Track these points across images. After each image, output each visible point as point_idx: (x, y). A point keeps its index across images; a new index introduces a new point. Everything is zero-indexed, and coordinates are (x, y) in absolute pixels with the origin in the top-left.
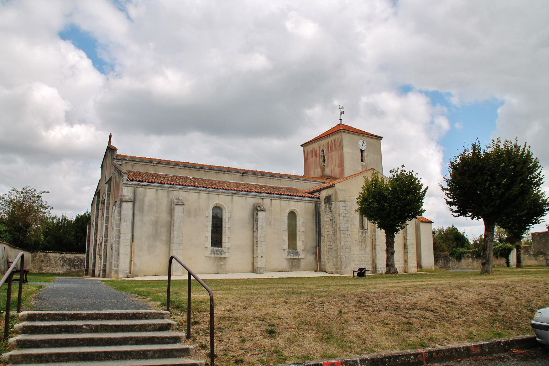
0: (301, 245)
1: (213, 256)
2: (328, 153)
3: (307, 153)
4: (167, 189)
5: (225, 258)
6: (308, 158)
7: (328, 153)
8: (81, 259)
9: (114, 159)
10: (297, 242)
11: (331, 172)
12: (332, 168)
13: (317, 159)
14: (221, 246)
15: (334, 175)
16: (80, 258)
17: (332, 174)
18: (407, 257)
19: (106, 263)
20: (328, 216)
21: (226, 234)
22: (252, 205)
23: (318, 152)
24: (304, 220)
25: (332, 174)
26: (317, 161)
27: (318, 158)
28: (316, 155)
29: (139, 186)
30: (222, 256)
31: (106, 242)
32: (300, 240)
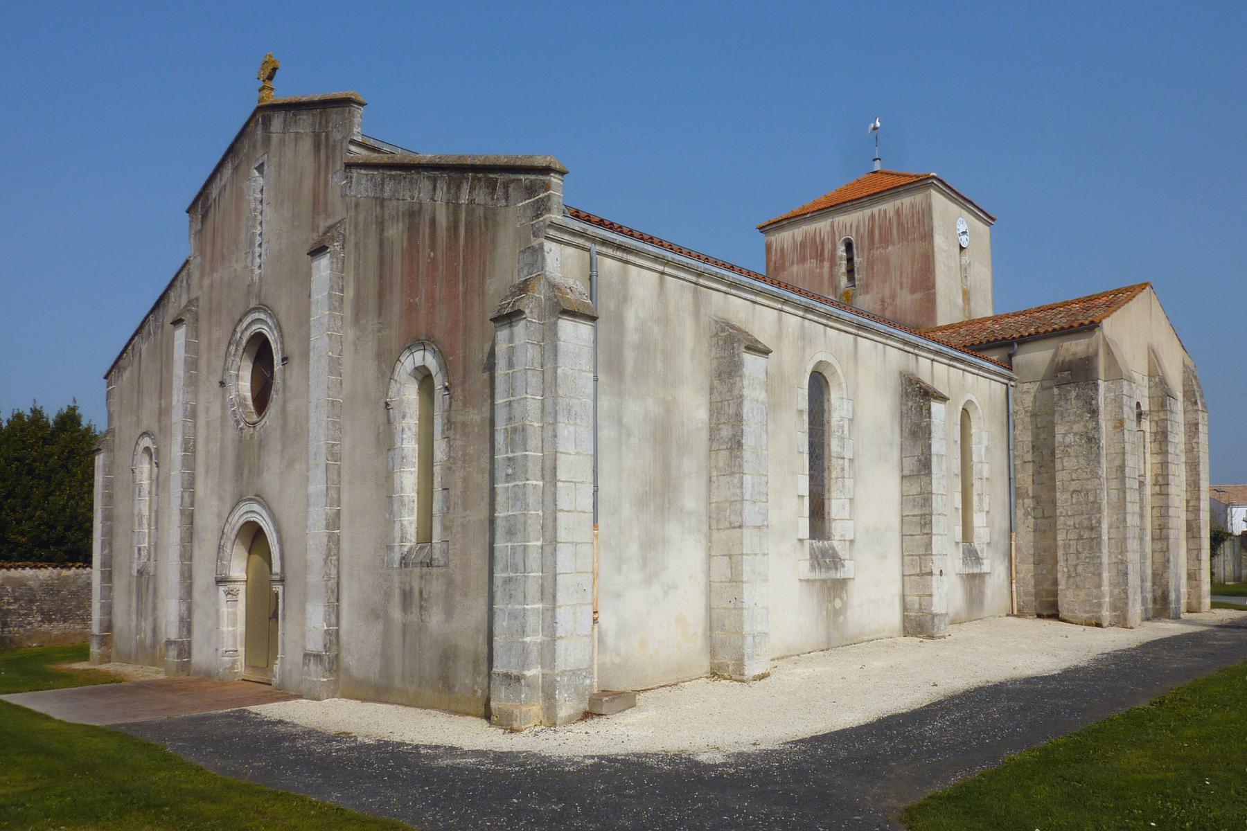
0: (985, 525)
1: (818, 575)
2: (870, 249)
3: (782, 249)
4: (694, 279)
5: (843, 582)
6: (784, 263)
7: (870, 249)
8: (31, 589)
9: (353, 142)
10: (974, 514)
11: (883, 305)
12: (887, 293)
13: (821, 268)
14: (829, 539)
15: (895, 313)
16: (26, 585)
17: (884, 310)
18: (1196, 562)
19: (338, 625)
20: (1077, 428)
21: (843, 486)
22: (897, 375)
23: (828, 246)
24: (988, 441)
25: (884, 310)
26: (821, 274)
27: (826, 264)
28: (819, 257)
29: (604, 250)
30: (838, 576)
31: (334, 524)
32: (981, 511)
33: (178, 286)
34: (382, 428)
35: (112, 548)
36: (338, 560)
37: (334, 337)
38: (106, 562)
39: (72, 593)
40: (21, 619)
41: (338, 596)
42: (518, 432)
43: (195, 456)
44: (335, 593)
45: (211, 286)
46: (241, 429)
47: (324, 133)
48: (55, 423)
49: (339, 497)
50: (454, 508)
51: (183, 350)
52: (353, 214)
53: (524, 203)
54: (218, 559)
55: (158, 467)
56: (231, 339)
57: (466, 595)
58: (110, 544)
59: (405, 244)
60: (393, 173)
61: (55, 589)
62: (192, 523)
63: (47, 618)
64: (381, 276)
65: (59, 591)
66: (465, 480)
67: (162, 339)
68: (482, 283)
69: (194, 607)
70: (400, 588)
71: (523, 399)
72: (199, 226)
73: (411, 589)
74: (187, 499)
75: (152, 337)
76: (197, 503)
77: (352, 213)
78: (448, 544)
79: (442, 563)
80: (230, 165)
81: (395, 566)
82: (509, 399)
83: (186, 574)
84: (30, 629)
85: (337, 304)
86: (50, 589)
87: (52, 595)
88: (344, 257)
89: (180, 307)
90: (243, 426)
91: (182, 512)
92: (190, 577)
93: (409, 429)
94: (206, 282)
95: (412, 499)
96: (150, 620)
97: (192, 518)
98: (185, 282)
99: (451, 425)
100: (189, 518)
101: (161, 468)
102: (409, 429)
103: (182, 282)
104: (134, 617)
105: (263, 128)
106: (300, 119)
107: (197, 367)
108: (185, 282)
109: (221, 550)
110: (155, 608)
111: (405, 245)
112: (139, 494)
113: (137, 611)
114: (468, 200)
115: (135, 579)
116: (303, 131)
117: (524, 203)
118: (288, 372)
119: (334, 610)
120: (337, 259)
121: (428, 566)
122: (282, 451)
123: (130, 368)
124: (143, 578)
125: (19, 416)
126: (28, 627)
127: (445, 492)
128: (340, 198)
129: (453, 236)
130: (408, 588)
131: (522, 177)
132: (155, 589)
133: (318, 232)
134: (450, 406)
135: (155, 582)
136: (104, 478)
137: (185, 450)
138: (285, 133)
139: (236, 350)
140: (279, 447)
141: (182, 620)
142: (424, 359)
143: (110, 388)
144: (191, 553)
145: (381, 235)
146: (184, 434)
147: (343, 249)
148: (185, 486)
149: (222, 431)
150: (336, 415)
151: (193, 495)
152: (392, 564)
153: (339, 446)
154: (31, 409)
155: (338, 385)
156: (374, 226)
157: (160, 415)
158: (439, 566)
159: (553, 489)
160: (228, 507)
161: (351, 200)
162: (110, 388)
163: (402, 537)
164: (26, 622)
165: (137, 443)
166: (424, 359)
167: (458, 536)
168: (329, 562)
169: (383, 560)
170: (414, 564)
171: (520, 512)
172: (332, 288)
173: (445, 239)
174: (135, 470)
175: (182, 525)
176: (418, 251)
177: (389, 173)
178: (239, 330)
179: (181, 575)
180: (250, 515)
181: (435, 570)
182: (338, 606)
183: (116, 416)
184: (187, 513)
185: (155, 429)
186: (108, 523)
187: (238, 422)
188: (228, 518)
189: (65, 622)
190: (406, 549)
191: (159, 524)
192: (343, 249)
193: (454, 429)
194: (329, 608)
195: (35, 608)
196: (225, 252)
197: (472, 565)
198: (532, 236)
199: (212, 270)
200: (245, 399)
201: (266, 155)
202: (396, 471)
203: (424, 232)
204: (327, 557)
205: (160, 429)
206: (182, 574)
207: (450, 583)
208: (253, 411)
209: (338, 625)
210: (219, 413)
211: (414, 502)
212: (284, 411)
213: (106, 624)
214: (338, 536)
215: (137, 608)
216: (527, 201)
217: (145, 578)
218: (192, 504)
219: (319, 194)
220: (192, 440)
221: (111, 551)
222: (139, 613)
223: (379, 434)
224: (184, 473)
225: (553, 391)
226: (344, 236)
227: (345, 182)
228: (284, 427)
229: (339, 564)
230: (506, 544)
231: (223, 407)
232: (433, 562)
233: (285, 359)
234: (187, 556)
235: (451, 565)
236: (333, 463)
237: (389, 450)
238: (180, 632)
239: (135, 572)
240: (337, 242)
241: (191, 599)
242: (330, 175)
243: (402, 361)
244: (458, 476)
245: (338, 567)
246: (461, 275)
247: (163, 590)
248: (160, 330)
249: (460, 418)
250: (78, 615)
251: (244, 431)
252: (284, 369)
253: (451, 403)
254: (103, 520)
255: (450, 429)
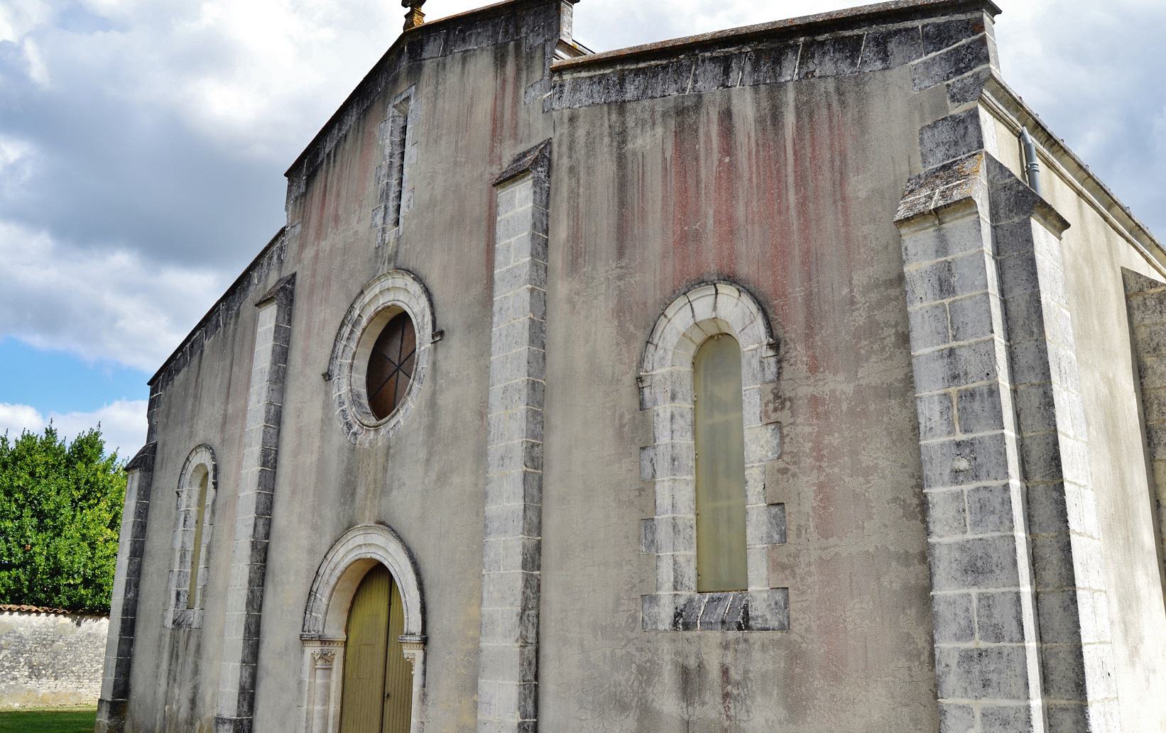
16: (15, 632)
33: (265, 264)
34: (627, 417)
35: (138, 591)
36: (538, 616)
37: (535, 292)
38: (130, 609)
39: (69, 644)
40: (4, 673)
41: (537, 671)
42: (978, 398)
43: (275, 473)
44: (533, 667)
45: (316, 256)
46: (355, 434)
47: (512, 43)
48: (73, 446)
49: (540, 522)
50: (799, 536)
51: (271, 336)
52: (566, 131)
53: (924, 58)
54: (306, 610)
55: (216, 488)
56: (346, 317)
57: (837, 678)
58: (137, 585)
59: (669, 153)
60: (642, 65)
61: (49, 638)
62: (265, 560)
63: (35, 672)
64: (622, 204)
65: (53, 641)
66: (825, 491)
67: (235, 330)
68: (841, 180)
69: (261, 673)
70: (676, 664)
71: (985, 342)
72: (303, 189)
73: (701, 666)
74: (261, 529)
75: (221, 330)
76: (273, 535)
77: (564, 129)
78: (787, 596)
79: (774, 623)
80: (354, 110)
81: (661, 627)
82: (947, 346)
83: (253, 627)
84: (12, 686)
85: (540, 249)
86: (44, 641)
87: (44, 645)
88: (549, 188)
89: (265, 288)
90: (358, 430)
91: (254, 546)
92: (258, 633)
93: (682, 416)
94: (309, 253)
95: (689, 524)
96: (187, 688)
97: (266, 553)
98: (275, 257)
99: (783, 403)
100: (262, 553)
101: (219, 489)
102: (682, 416)
103: (271, 258)
104: (163, 681)
105: (410, 58)
106: (471, 34)
107: (286, 359)
108: (275, 257)
109: (313, 598)
110: (196, 671)
111: (668, 155)
112: (184, 524)
113: (169, 674)
114: (798, 74)
115: (169, 632)
116: (476, 47)
117: (924, 58)
118: (441, 355)
119: (531, 692)
120: (541, 188)
121: (740, 628)
122: (428, 460)
123: (185, 369)
124: (181, 631)
125: (28, 437)
126: (12, 683)
127: (775, 510)
128: (541, 116)
129: (769, 127)
130: (692, 663)
131: (918, 23)
132: (199, 646)
133: (501, 164)
134: (779, 374)
135: (199, 637)
136: (137, 502)
137: (264, 464)
138: (446, 56)
139: (352, 332)
140: (422, 454)
141: (242, 690)
142: (715, 308)
143: (155, 395)
144: (261, 601)
145: (620, 148)
146: (264, 443)
147: (549, 177)
148: (260, 511)
149: (322, 438)
150: (538, 403)
151: (269, 524)
152: (655, 623)
153: (540, 446)
154: (46, 429)
155: (541, 360)
156: (607, 140)
157: (224, 423)
158: (767, 629)
159: (1055, 495)
160: (327, 540)
161: (562, 114)
162: (155, 395)
163: (676, 582)
164: (9, 676)
165: (188, 459)
166: (715, 308)
167: (810, 580)
168: (525, 618)
169: (635, 619)
170: (708, 625)
171: (998, 534)
172: (534, 226)
173: (753, 134)
174: (180, 493)
175: (252, 563)
176: (697, 159)
177: (633, 67)
178: (358, 306)
179: (245, 629)
180: (364, 550)
181: (755, 636)
182: (536, 686)
183: (159, 429)
184: (259, 547)
185: (216, 441)
186: (137, 560)
187: (349, 426)
188: (328, 553)
189: (56, 679)
190: (682, 601)
191: (211, 561)
192: (549, 177)
193: (791, 407)
194: (525, 689)
195: (22, 660)
196: (340, 213)
197: (850, 627)
198: (948, 102)
199: (319, 237)
200: (359, 396)
201: (413, 87)
202: (748, 466)
203: (708, 135)
204: (524, 610)
205: (223, 441)
206: (247, 628)
207: (795, 656)
208: (370, 411)
209: (536, 716)
210: (318, 414)
211: (692, 527)
212: (432, 405)
213: (121, 688)
214: (539, 580)
215: (170, 670)
216: (934, 54)
217: (184, 631)
218: (267, 536)
219: (502, 116)
220: (273, 452)
221: (137, 595)
222: (172, 677)
223: (622, 426)
224: (260, 493)
225: (1035, 330)
226: (550, 160)
227: (549, 94)
228: (432, 428)
229: (538, 624)
230: (965, 591)
231: (327, 406)
232: (751, 623)
233: (438, 334)
234: (256, 603)
235: (796, 627)
236: (533, 470)
237: (643, 448)
238: (239, 707)
239: (169, 623)
240: (541, 166)
241: (256, 663)
242: (523, 91)
243: (669, 316)
244: (806, 484)
245: (538, 627)
246: (791, 179)
247: (210, 646)
248: (233, 320)
249: (804, 391)
250: (73, 672)
251: (359, 437)
252: (435, 349)
253: (780, 368)
254: (130, 556)
255: (782, 408)
